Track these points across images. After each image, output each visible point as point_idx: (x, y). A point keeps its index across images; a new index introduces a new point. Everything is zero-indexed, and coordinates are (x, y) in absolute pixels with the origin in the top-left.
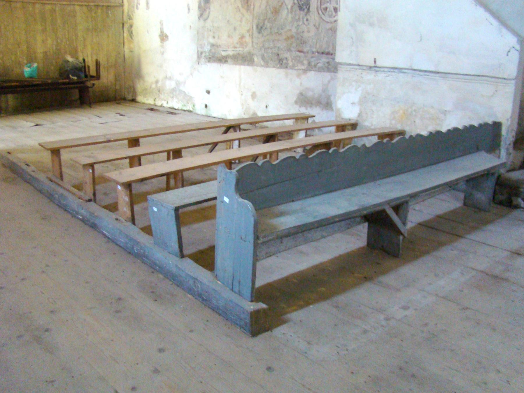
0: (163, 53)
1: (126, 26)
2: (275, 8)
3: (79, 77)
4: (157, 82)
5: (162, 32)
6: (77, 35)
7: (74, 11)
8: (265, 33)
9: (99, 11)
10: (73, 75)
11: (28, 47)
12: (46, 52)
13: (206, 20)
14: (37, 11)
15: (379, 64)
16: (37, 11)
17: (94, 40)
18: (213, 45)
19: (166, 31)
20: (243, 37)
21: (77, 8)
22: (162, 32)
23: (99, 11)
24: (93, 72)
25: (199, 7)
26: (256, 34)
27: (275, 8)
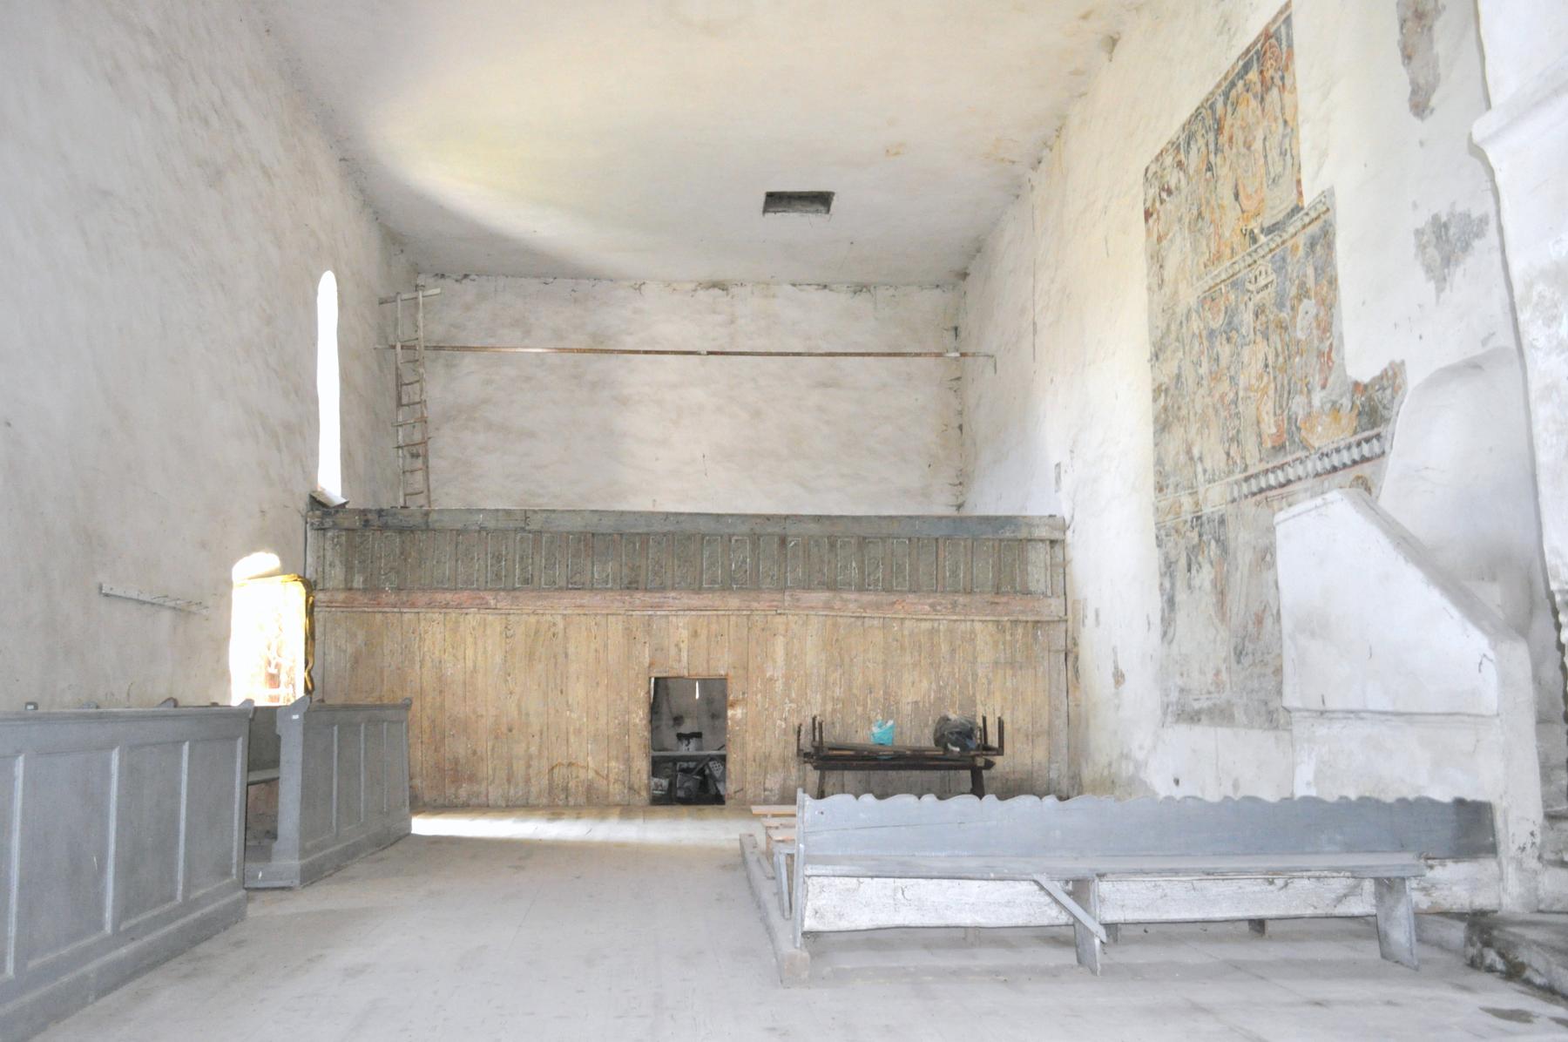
0: (1118, 707)
1: (1071, 659)
2: (1256, 615)
3: (964, 748)
4: (1110, 765)
5: (1116, 668)
6: (975, 675)
7: (973, 632)
8: (1246, 661)
9: (1020, 630)
10: (955, 745)
11: (885, 693)
12: (916, 703)
13: (1171, 642)
14: (906, 633)
15: (1330, 705)
16: (906, 633)
17: (1008, 684)
18: (1182, 690)
19: (1122, 667)
20: (1217, 674)
21: (978, 626)
22: (1116, 668)
23: (1020, 630)
24: (993, 740)
25: (1163, 619)
26: (1234, 666)
27: (1256, 615)
